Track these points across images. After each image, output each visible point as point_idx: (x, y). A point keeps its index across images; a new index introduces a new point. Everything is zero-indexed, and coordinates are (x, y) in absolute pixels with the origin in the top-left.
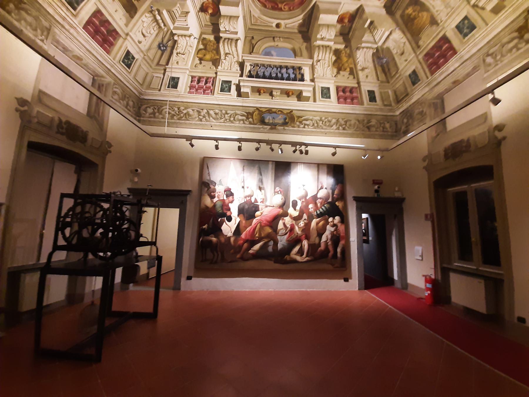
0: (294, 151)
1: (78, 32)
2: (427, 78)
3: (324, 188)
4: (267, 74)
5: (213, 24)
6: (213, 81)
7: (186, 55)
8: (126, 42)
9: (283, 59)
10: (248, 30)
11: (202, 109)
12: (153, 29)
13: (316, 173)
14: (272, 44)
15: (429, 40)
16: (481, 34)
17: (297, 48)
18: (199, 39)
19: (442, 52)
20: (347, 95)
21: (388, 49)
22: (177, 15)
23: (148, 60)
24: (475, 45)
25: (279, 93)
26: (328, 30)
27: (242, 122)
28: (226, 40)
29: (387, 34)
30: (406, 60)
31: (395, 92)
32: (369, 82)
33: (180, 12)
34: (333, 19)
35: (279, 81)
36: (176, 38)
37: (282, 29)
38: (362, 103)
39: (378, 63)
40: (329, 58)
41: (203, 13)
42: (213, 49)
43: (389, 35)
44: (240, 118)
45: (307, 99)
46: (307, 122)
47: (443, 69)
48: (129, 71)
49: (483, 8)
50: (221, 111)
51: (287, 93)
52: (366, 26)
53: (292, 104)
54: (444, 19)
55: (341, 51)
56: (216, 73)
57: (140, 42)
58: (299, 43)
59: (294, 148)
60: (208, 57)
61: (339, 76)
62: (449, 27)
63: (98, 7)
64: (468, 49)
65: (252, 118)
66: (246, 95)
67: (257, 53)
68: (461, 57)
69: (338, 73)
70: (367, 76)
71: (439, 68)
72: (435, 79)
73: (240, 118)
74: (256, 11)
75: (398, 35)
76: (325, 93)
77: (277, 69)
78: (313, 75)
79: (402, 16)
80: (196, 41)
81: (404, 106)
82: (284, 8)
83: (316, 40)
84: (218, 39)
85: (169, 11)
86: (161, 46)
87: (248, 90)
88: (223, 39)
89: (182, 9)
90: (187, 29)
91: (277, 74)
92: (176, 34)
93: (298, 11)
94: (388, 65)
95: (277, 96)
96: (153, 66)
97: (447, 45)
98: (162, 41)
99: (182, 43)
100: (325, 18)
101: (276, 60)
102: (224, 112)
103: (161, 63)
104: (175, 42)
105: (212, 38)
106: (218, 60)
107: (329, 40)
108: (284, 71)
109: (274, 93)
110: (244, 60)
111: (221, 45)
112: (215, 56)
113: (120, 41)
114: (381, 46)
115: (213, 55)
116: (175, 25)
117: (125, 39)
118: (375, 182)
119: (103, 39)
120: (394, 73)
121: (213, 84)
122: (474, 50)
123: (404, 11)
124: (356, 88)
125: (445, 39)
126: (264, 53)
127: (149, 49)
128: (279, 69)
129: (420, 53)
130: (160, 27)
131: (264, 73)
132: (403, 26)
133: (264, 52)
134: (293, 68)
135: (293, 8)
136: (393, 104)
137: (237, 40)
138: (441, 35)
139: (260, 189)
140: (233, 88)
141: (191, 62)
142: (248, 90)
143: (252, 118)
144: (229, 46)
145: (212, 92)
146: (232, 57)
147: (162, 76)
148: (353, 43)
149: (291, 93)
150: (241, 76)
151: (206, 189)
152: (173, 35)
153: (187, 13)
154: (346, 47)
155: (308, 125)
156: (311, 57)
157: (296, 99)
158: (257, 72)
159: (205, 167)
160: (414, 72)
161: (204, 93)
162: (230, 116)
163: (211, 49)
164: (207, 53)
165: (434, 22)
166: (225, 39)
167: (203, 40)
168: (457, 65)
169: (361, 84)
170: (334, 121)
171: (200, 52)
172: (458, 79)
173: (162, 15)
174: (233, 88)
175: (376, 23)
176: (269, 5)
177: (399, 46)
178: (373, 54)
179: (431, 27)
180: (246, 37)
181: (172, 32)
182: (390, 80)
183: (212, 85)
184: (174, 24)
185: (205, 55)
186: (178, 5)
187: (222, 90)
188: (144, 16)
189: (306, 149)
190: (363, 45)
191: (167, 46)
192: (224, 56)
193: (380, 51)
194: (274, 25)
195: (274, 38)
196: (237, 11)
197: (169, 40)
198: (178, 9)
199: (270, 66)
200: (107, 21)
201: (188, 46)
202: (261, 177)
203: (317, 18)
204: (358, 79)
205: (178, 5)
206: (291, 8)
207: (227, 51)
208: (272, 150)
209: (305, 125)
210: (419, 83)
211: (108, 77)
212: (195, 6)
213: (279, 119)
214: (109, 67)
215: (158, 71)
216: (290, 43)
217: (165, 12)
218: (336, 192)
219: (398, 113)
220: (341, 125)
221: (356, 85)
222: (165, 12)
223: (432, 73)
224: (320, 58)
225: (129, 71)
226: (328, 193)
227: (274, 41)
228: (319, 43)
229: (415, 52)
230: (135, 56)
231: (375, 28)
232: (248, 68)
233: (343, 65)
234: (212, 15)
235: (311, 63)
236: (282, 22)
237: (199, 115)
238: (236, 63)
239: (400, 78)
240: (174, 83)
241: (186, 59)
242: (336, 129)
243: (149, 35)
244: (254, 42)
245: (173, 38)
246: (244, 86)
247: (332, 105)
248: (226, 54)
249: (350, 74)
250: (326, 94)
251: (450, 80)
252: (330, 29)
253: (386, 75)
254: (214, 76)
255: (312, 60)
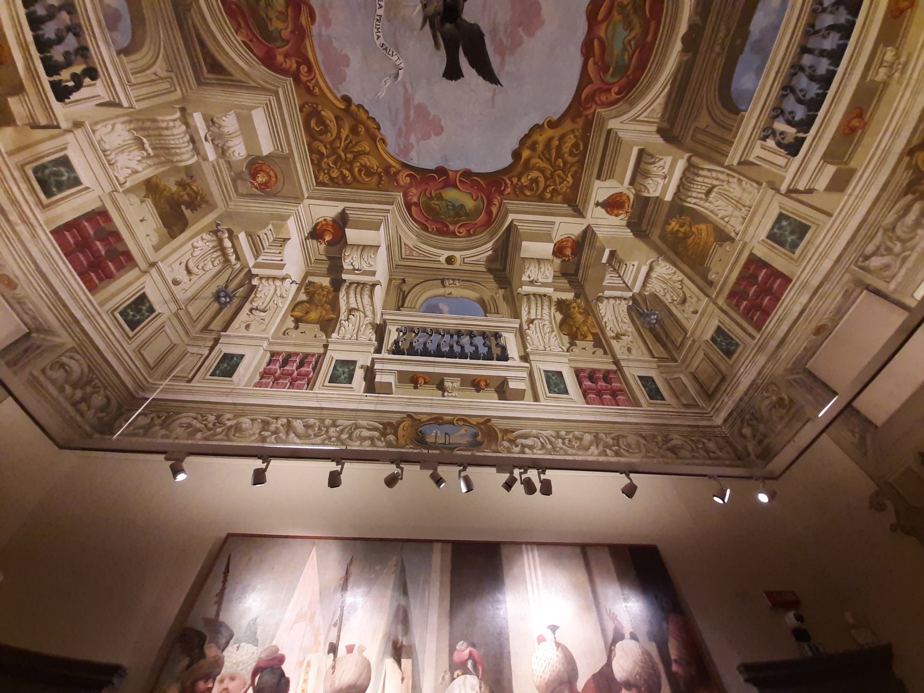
0: (508, 486)
1: (34, 235)
2: (753, 337)
3: (627, 636)
4: (432, 347)
5: (330, 258)
6: (317, 362)
7: (270, 313)
8: (146, 278)
9: (462, 319)
10: (393, 267)
11: (277, 418)
12: (213, 262)
13: (582, 576)
14: (441, 291)
15: (726, 269)
16: (877, 148)
17: (487, 298)
18: (301, 284)
19: (758, 290)
20: (600, 385)
21: (654, 296)
22: (266, 244)
23: (186, 320)
24: (824, 256)
25: (457, 385)
26: (540, 268)
27: (368, 443)
28: (354, 286)
29: (644, 269)
30: (696, 312)
31: (694, 377)
32: (637, 363)
33: (271, 239)
34: (546, 249)
35: (458, 360)
36: (255, 282)
37: (457, 266)
38: (637, 404)
39: (643, 325)
40: (549, 316)
41: (315, 241)
42: (326, 302)
43: (648, 271)
44: (366, 433)
45: (519, 395)
46: (529, 442)
47: (779, 312)
48: (131, 334)
49: (810, 191)
50: (322, 421)
51: (477, 384)
52: (604, 260)
53: (486, 405)
54: (740, 228)
55: (571, 304)
56: (326, 347)
57: (176, 283)
58: (490, 289)
59: (505, 476)
60: (313, 315)
61: (575, 349)
62: (756, 239)
63: (104, 205)
64: (812, 268)
65: (396, 435)
66: (387, 389)
67: (412, 308)
68: (804, 286)
69: (572, 344)
70: (629, 350)
71: (767, 313)
72: (772, 336)
73: (366, 433)
74: (410, 237)
75: (664, 269)
76: (555, 382)
77: (452, 336)
78: (525, 347)
79: (663, 237)
80: (294, 287)
81: (729, 403)
82: (459, 232)
83: (522, 284)
84: (337, 284)
85: (249, 235)
86: (221, 297)
87: (391, 379)
88: (347, 284)
89: (278, 233)
90: (281, 267)
91: (451, 347)
92: (257, 275)
93: (484, 236)
94: (663, 327)
95: (453, 389)
96: (193, 333)
97: (764, 271)
98: (226, 286)
99: (266, 290)
100: (529, 248)
101: (448, 320)
102: (328, 422)
103: (211, 327)
104: (253, 288)
105: (326, 282)
106: (333, 322)
107: (544, 285)
108: (465, 340)
109: (448, 384)
110: (385, 321)
111: (342, 294)
112: (327, 313)
113: (135, 273)
114: (640, 294)
115: (324, 313)
116: (259, 260)
117: (145, 272)
118: (782, 602)
119: (76, 243)
120: (679, 340)
121: (316, 368)
122: (827, 264)
123: (663, 229)
124: (615, 372)
125: (754, 262)
126: (423, 308)
127: (193, 298)
128: (455, 337)
129: (718, 294)
130: (227, 261)
131: (425, 344)
132: (670, 254)
133: (425, 305)
134: (484, 334)
135: (475, 232)
136: (700, 402)
137: (373, 286)
138: (745, 255)
139: (398, 651)
140: (359, 374)
141: (276, 325)
142: (391, 379)
143: (396, 435)
144: (359, 296)
145: (311, 384)
146: (362, 314)
147: (207, 352)
148: (589, 289)
149: (483, 384)
150: (378, 350)
151: (186, 661)
152: (250, 276)
153: (286, 240)
154: (577, 296)
155: (531, 447)
156: (516, 315)
157: (496, 395)
158: (411, 343)
159: (220, 568)
160: (719, 330)
161: (292, 386)
162: (342, 432)
163: (320, 304)
164: (313, 308)
165: (723, 237)
166: (351, 284)
167: (307, 286)
168: (804, 299)
169: (623, 363)
170: (588, 438)
171: (299, 307)
172: (823, 322)
173: (235, 241)
174: (359, 374)
175: (620, 254)
176: (432, 226)
177: (673, 288)
178: (629, 308)
179: (721, 245)
180: (390, 280)
181: (250, 271)
182: (676, 355)
183: (314, 369)
184: (256, 257)
185: (307, 312)
186: (270, 227)
187: (334, 379)
188: (199, 237)
189: (543, 477)
190: (607, 293)
191: (233, 295)
192: (346, 314)
193: (640, 300)
194: (442, 259)
195: (443, 281)
196: (379, 237)
197: (240, 285)
198: (269, 233)
199: (437, 332)
200: (116, 235)
201: (277, 296)
202: (403, 601)
203: (518, 248)
204: (614, 356)
205: (270, 227)
206: (471, 231)
207: (354, 305)
208: (438, 481)
209: (523, 446)
210: (739, 350)
211: (65, 334)
212: (300, 228)
213: (461, 436)
214: (79, 315)
215: (200, 343)
216: (473, 289)
217: (242, 237)
218: (673, 654)
219: (719, 421)
220: (607, 446)
221: (614, 367)
222: (242, 237)
223: (759, 326)
224: (533, 317)
225: (131, 334)
226: (646, 653)
227: (444, 287)
228: (526, 289)
229: (707, 295)
230: (156, 307)
231: (620, 262)
232: (392, 335)
233: (578, 328)
234: (329, 243)
235: (518, 326)
236: (457, 254)
237: (264, 429)
238: (370, 327)
239: (696, 345)
240: (228, 366)
241: (267, 320)
242: (599, 455)
243: (201, 272)
244: (405, 288)
245: (250, 282)
246: (382, 371)
247: (573, 406)
248: (351, 311)
249: (595, 346)
250: (556, 385)
251: (806, 329)
252: (542, 266)
253: (664, 346)
254: (321, 351)
255: (518, 321)
